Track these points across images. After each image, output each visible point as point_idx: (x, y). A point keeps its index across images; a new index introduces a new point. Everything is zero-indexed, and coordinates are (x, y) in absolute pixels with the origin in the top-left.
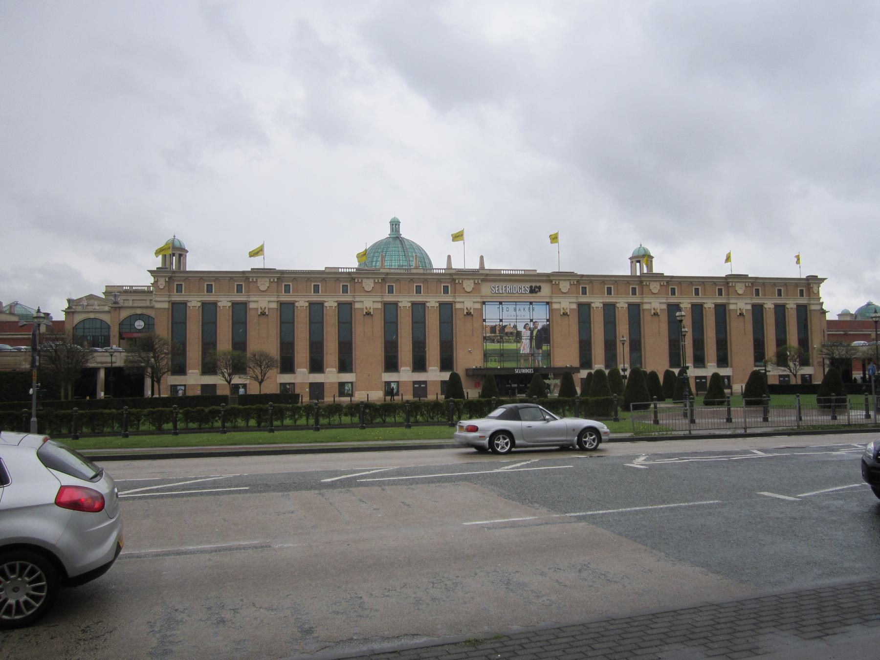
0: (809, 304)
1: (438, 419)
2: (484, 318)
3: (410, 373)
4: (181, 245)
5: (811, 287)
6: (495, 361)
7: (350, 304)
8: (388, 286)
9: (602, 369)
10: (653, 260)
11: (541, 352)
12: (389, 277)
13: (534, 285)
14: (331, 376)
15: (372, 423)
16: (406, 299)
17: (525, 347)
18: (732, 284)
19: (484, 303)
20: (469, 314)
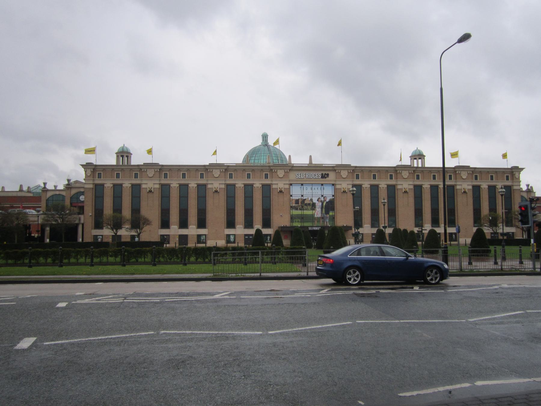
0: (513, 185)
1: (174, 260)
2: (291, 194)
3: (243, 229)
4: (127, 150)
5: (514, 174)
6: (298, 222)
7: (205, 185)
8: (229, 174)
9: (259, 228)
10: (425, 157)
11: (328, 216)
12: (229, 168)
13: (324, 173)
14: (192, 231)
15: (129, 262)
16: (383, 183)
17: (318, 213)
18: (458, 172)
19: (291, 184)
20: (281, 191)
